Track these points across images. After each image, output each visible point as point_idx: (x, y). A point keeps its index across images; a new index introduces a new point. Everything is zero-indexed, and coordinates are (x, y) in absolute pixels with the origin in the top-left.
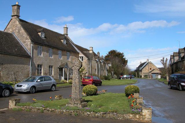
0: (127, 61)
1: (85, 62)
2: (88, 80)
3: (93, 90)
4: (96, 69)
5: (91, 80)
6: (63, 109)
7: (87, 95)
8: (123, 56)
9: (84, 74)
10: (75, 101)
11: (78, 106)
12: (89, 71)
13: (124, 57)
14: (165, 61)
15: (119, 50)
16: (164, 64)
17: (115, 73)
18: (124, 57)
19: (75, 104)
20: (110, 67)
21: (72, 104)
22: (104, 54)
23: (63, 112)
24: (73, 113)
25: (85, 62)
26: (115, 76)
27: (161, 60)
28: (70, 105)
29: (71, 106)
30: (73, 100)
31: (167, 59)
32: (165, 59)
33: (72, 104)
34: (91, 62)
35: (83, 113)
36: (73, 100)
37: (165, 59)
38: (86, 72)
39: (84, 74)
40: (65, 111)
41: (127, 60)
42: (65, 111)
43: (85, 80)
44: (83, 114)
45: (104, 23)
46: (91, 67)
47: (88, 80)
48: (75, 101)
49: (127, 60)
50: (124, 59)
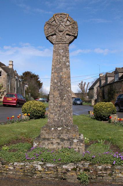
0: (42, 84)
1: (4, 78)
2: (11, 99)
3: (41, 109)
4: (15, 88)
5: (15, 99)
6: (30, 161)
7: (31, 118)
8: (38, 78)
9: (2, 93)
10: (61, 132)
11: (74, 146)
12: (8, 89)
13: (39, 80)
14: (83, 85)
15: (34, 72)
16: (82, 88)
17: (31, 95)
18: (39, 80)
19: (63, 140)
20: (27, 88)
21: (55, 141)
22: (20, 74)
23: (34, 170)
24: (74, 173)
25: (4, 78)
26: (32, 98)
27: (80, 84)
28: (46, 145)
29: (51, 147)
30: (56, 130)
31: (85, 83)
32: (83, 83)
33: (55, 141)
34: (11, 80)
35: (109, 172)
36: (56, 130)
37: (83, 83)
38: (5, 91)
39: (2, 93)
40: (40, 168)
41: (42, 83)
42: (40, 168)
43: (7, 99)
44: (111, 175)
45: (27, 44)
46: (11, 85)
47: (11, 99)
48: (61, 132)
49: (42, 83)
50: (39, 82)
